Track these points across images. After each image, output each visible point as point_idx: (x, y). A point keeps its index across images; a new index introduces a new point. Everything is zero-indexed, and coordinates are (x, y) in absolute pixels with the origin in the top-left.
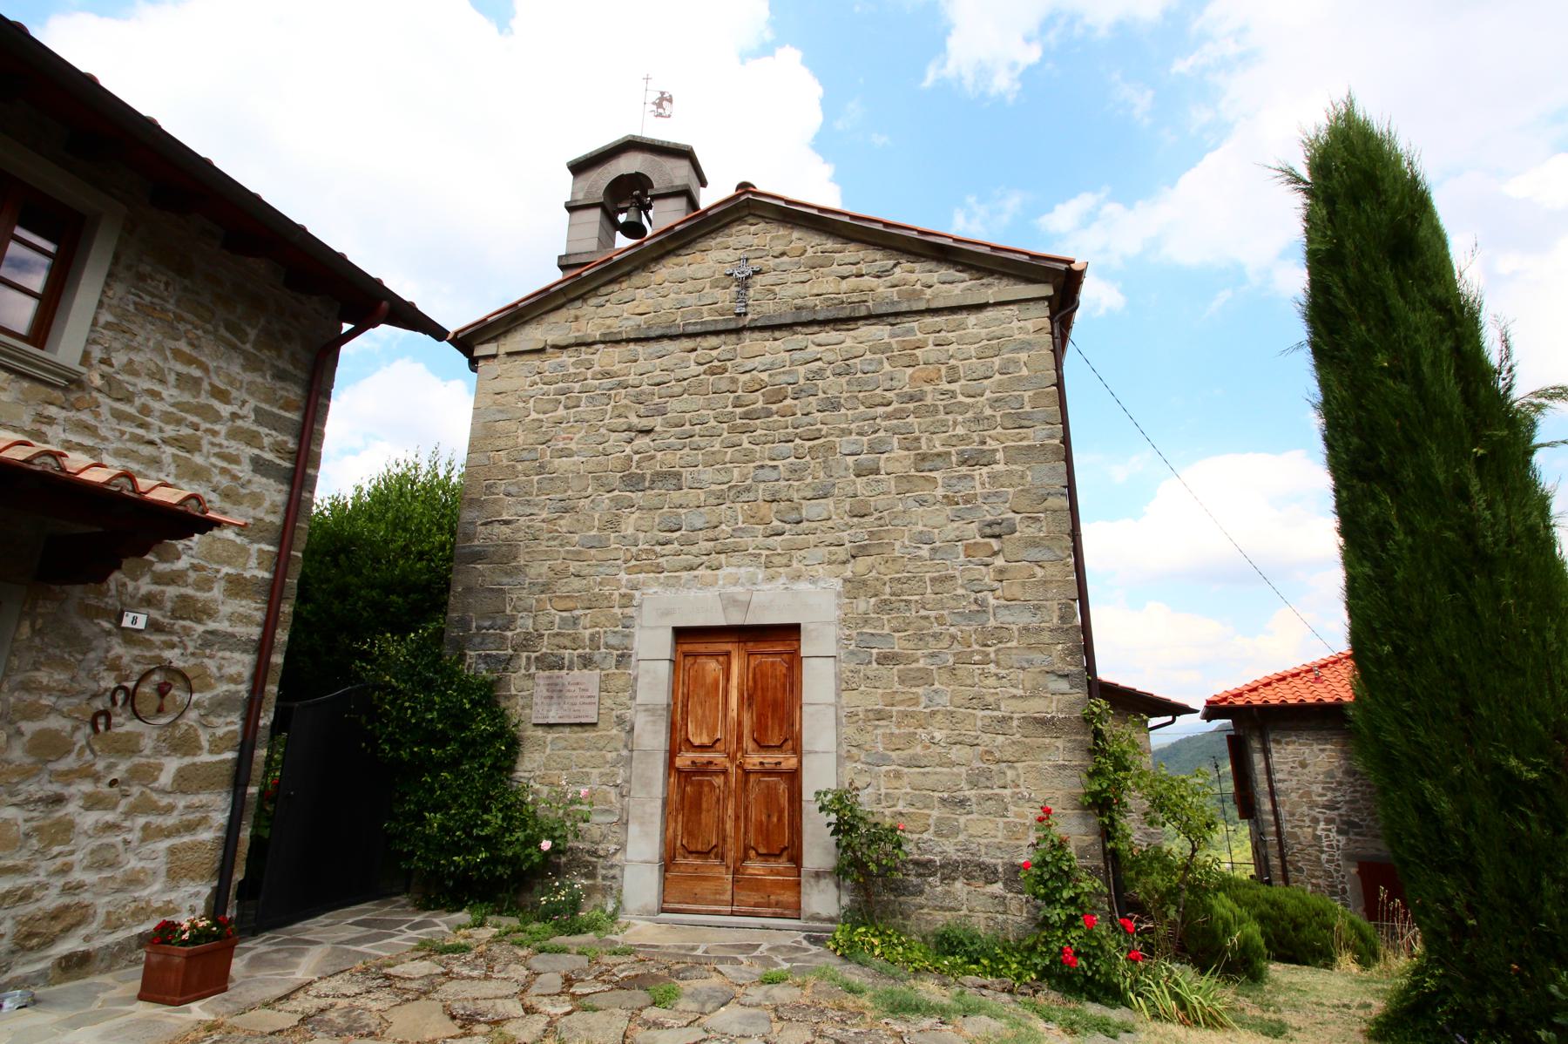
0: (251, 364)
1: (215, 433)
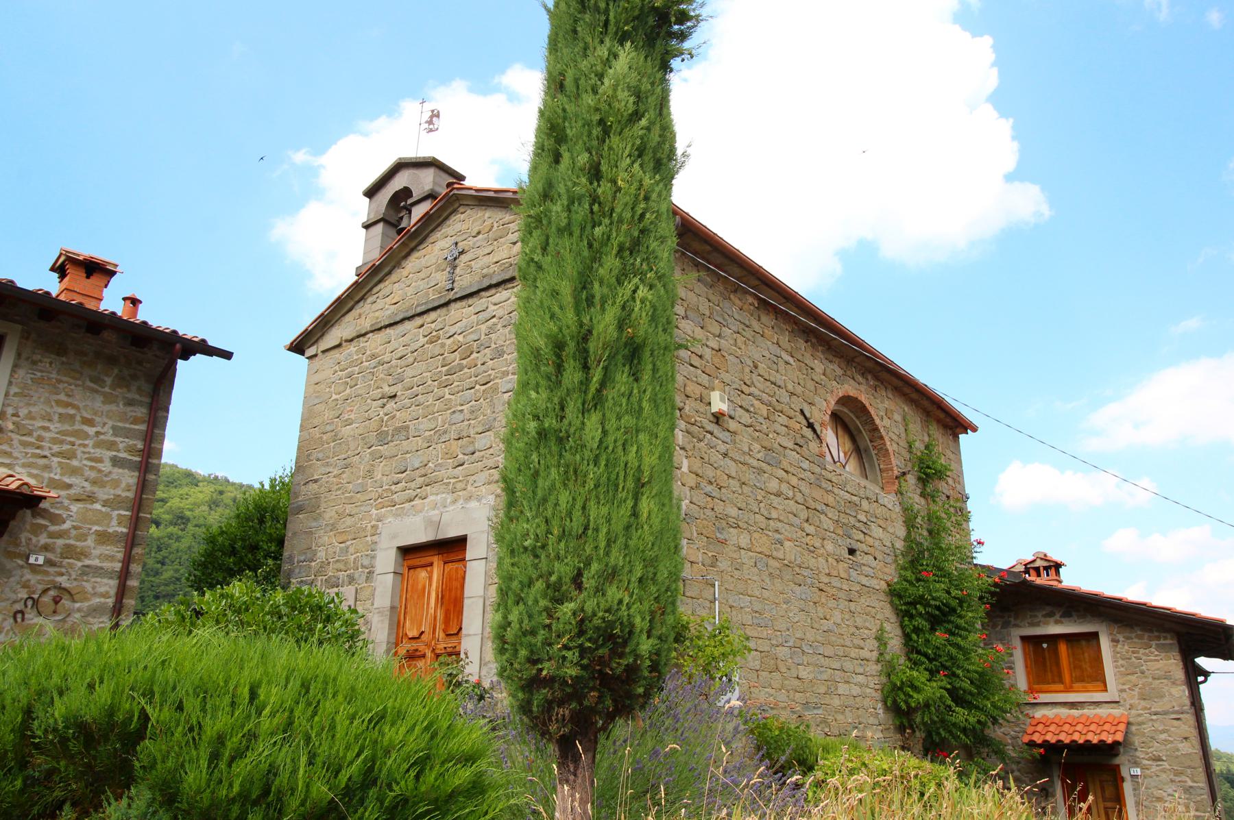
0: (108, 399)
1: (85, 446)
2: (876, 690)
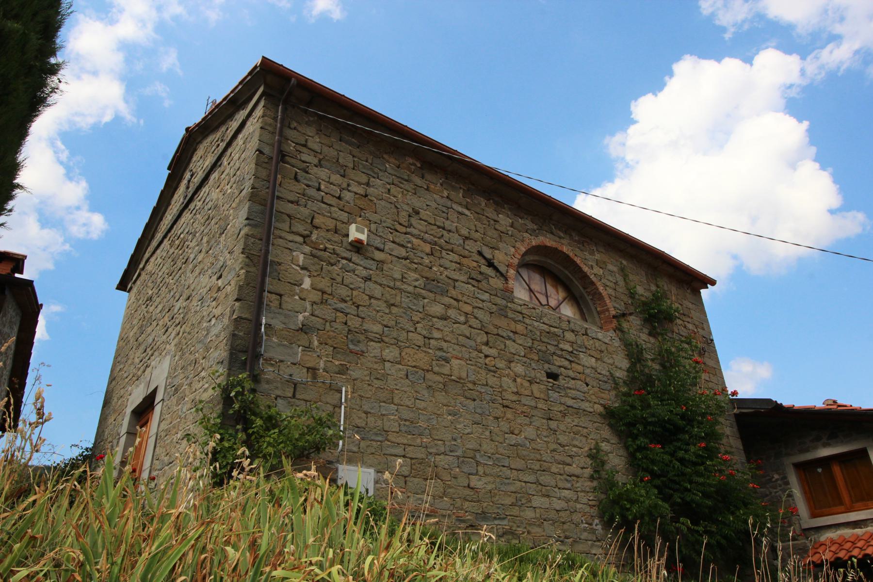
2: (591, 506)
